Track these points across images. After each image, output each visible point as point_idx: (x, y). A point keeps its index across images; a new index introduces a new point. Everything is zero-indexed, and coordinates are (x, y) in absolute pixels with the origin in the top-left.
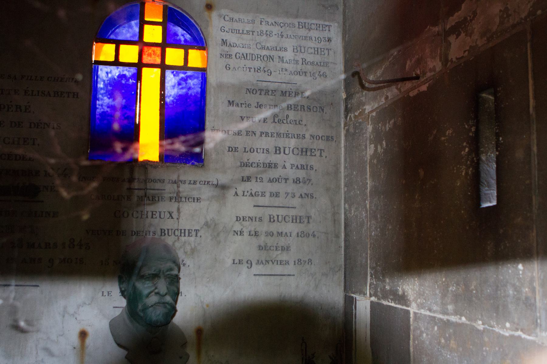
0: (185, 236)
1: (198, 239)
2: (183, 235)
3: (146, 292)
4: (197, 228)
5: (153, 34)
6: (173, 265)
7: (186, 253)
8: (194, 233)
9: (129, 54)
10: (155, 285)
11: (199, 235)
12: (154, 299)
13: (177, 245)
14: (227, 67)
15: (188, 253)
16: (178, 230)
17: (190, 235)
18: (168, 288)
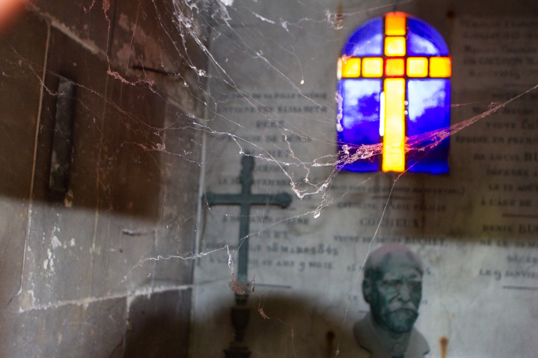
3: (389, 297)
5: (396, 46)
7: (431, 261)
9: (373, 67)
12: (396, 305)
13: (422, 253)
14: (472, 74)
18: (411, 295)
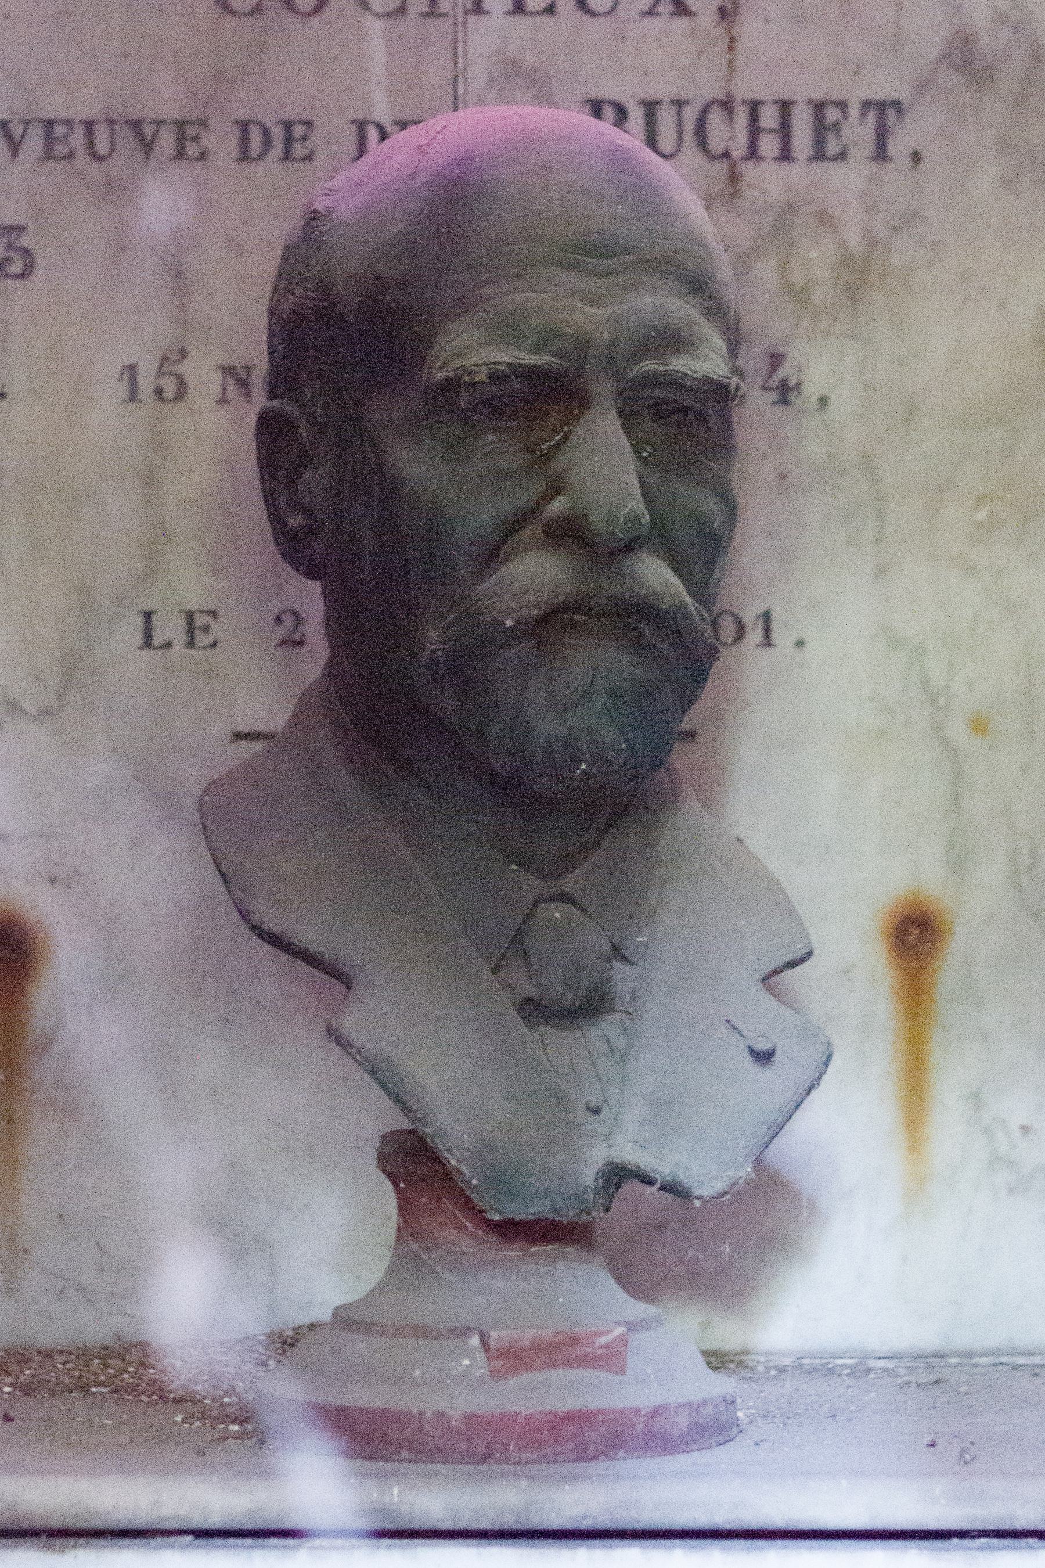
0: (786, 155)
1: (895, 174)
2: (769, 145)
3: (482, 514)
4: (883, 88)
6: (682, 310)
8: (858, 132)
10: (546, 458)
11: (899, 146)
15: (818, 296)
16: (727, 105)
17: (832, 147)
